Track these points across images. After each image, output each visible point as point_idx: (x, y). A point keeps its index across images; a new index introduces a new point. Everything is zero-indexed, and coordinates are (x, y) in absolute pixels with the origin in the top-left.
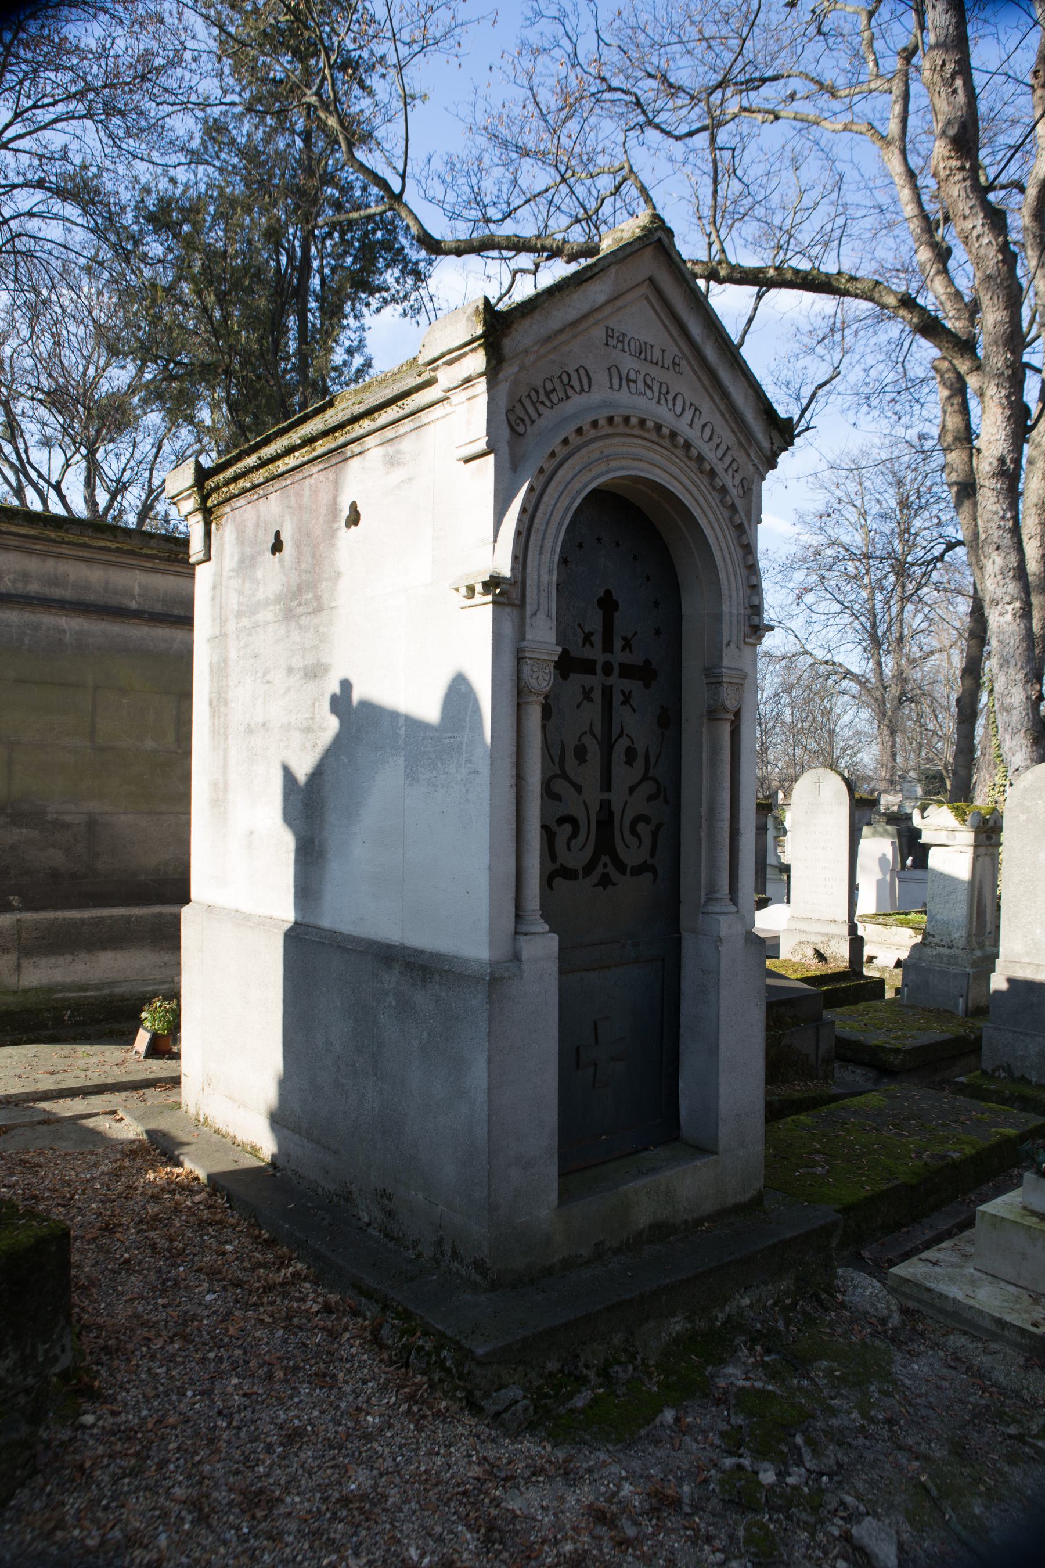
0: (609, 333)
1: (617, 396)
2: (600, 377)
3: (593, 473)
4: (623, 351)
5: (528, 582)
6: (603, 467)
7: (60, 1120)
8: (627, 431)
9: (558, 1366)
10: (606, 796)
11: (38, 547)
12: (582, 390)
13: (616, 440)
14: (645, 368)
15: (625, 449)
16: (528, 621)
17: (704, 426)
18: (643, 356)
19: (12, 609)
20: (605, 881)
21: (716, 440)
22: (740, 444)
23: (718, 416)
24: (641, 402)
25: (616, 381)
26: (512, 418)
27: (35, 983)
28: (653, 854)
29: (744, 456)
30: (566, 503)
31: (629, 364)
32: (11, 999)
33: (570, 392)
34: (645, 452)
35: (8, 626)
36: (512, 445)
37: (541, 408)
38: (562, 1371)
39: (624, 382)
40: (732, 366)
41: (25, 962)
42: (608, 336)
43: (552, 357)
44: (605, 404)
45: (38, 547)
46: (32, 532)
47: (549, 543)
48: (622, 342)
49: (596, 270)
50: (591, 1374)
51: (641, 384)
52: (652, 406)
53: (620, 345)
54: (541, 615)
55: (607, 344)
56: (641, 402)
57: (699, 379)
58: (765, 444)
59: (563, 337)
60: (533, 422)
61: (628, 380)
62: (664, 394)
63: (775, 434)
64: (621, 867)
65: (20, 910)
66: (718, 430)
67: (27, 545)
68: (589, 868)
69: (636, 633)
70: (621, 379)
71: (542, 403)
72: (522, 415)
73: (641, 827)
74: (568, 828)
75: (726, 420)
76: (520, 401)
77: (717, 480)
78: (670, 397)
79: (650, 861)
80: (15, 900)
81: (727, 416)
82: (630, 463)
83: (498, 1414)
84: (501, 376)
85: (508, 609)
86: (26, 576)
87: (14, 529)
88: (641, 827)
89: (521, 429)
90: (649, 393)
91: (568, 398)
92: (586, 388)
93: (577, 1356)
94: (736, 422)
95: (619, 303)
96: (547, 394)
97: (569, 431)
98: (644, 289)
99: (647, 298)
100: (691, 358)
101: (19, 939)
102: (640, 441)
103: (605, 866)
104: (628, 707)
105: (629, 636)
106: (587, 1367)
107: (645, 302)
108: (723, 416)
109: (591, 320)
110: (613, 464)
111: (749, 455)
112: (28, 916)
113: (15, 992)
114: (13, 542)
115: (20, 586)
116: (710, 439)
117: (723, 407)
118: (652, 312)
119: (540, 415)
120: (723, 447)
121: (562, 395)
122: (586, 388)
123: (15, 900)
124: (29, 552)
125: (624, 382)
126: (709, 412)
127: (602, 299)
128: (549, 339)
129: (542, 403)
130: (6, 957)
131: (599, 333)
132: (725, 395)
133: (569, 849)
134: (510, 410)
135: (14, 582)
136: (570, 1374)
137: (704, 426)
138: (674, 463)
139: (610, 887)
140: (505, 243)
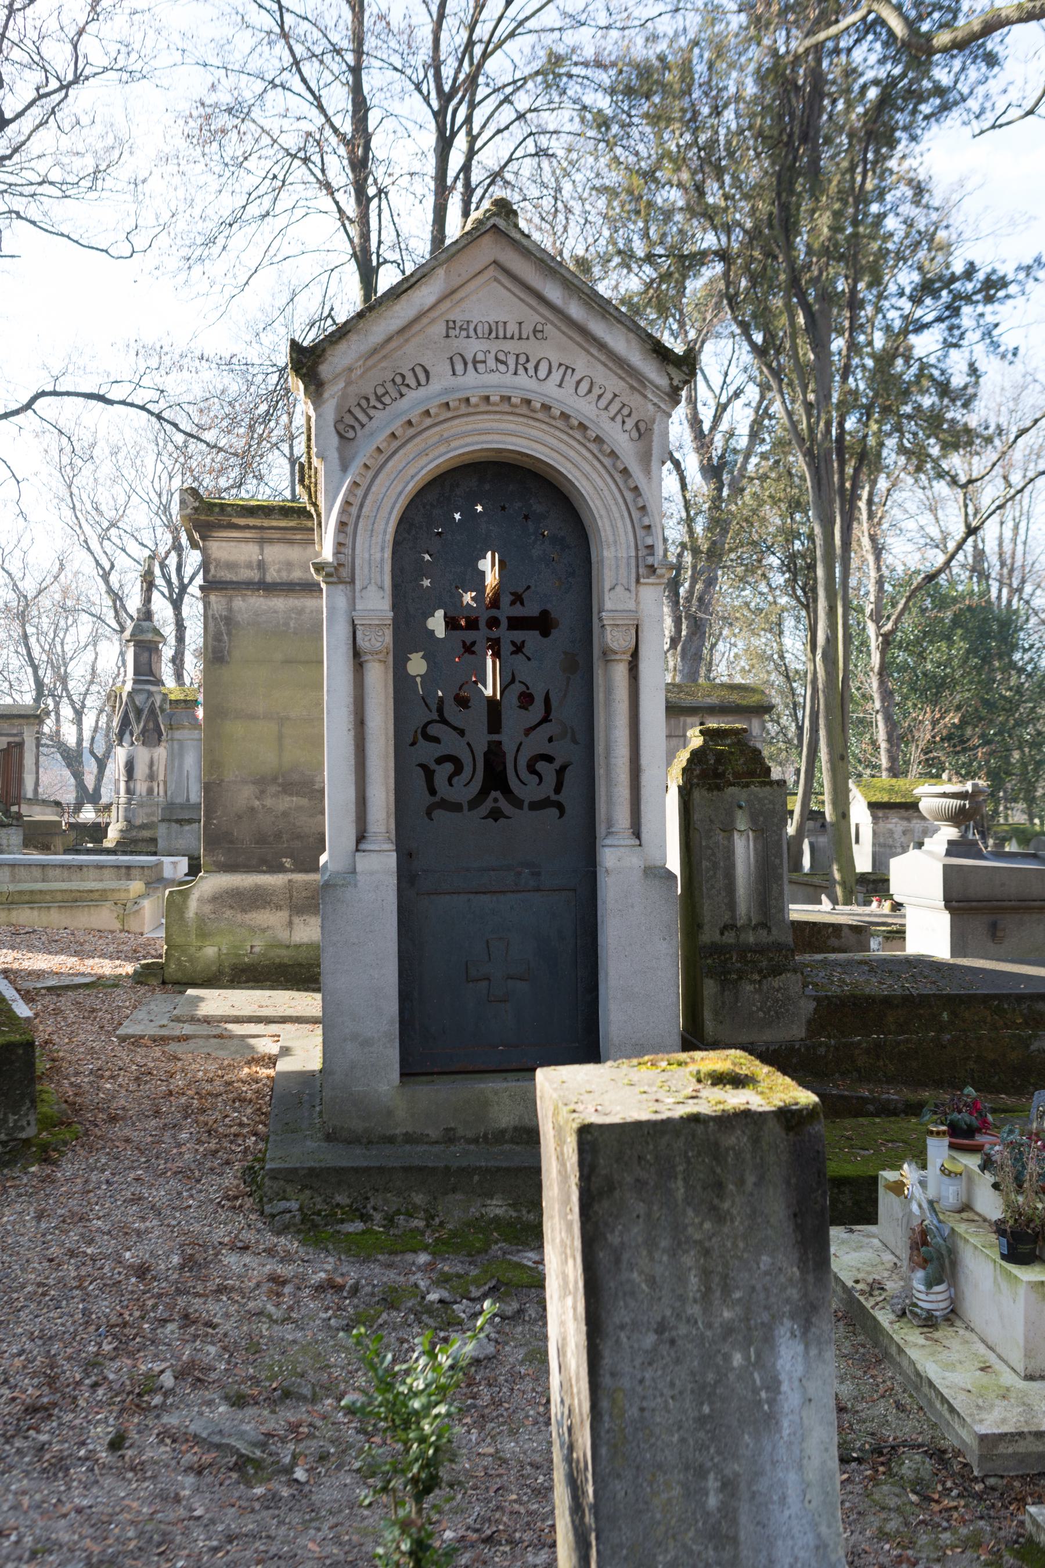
0: (450, 325)
1: (460, 380)
2: (440, 369)
3: (431, 456)
4: (468, 337)
5: (358, 562)
6: (443, 449)
7: (232, 1037)
8: (471, 410)
9: (348, 1201)
10: (495, 737)
11: (299, 537)
12: (419, 385)
13: (457, 422)
14: (494, 346)
15: (470, 427)
16: (357, 594)
17: (578, 383)
18: (493, 335)
19: (278, 596)
20: (496, 814)
21: (597, 391)
22: (632, 387)
23: (600, 367)
24: (494, 379)
25: (459, 367)
26: (341, 427)
27: (305, 940)
28: (558, 790)
29: (639, 398)
30: (399, 489)
31: (473, 347)
32: (284, 952)
33: (404, 390)
34: (495, 425)
35: (276, 612)
36: (341, 450)
37: (372, 412)
38: (351, 1206)
39: (470, 366)
40: (604, 317)
41: (296, 920)
42: (448, 328)
43: (384, 364)
44: (446, 391)
45: (299, 537)
46: (292, 524)
47: (380, 526)
48: (467, 329)
49: (413, 280)
50: (378, 1217)
51: (491, 363)
52: (509, 379)
53: (464, 333)
54: (372, 588)
55: (447, 336)
56: (494, 379)
57: (570, 338)
58: (663, 382)
59: (393, 344)
60: (363, 426)
61: (475, 362)
62: (522, 363)
63: (672, 370)
64: (518, 803)
65: (292, 871)
66: (599, 380)
67: (288, 536)
68: (474, 804)
69: (529, 587)
70: (466, 364)
71: (374, 407)
72: (352, 422)
73: (541, 766)
74: (449, 767)
75: (610, 369)
76: (349, 411)
77: (589, 432)
78: (530, 366)
79: (554, 797)
80: (287, 862)
81: (610, 364)
82: (476, 438)
83: (273, 1216)
84: (326, 395)
85: (341, 587)
86: (289, 565)
87: (274, 523)
88: (541, 766)
89: (351, 434)
90: (502, 368)
91: (402, 395)
92: (423, 381)
93: (367, 1198)
94: (623, 368)
95: (457, 296)
96: (379, 399)
97: (396, 426)
98: (491, 272)
99: (496, 280)
100: (556, 321)
101: (291, 898)
102: (486, 417)
103: (496, 800)
104: (520, 656)
105: (520, 590)
106: (375, 1209)
107: (495, 284)
108: (605, 365)
109: (425, 321)
110: (453, 445)
111: (645, 397)
112: (299, 877)
113: (288, 947)
114: (277, 535)
115: (284, 574)
116: (590, 391)
117: (603, 358)
118: (505, 291)
119: (371, 418)
120: (609, 396)
121: (394, 394)
122: (423, 381)
123: (287, 862)
124: (291, 542)
125: (470, 366)
126: (583, 364)
127: (431, 300)
128: (375, 351)
129: (374, 407)
130: (280, 914)
131: (440, 328)
132: (602, 346)
133: (451, 785)
134: (339, 421)
135: (279, 571)
136: (357, 1210)
137: (578, 383)
138: (533, 427)
139: (502, 820)
140: (1015, 15)
